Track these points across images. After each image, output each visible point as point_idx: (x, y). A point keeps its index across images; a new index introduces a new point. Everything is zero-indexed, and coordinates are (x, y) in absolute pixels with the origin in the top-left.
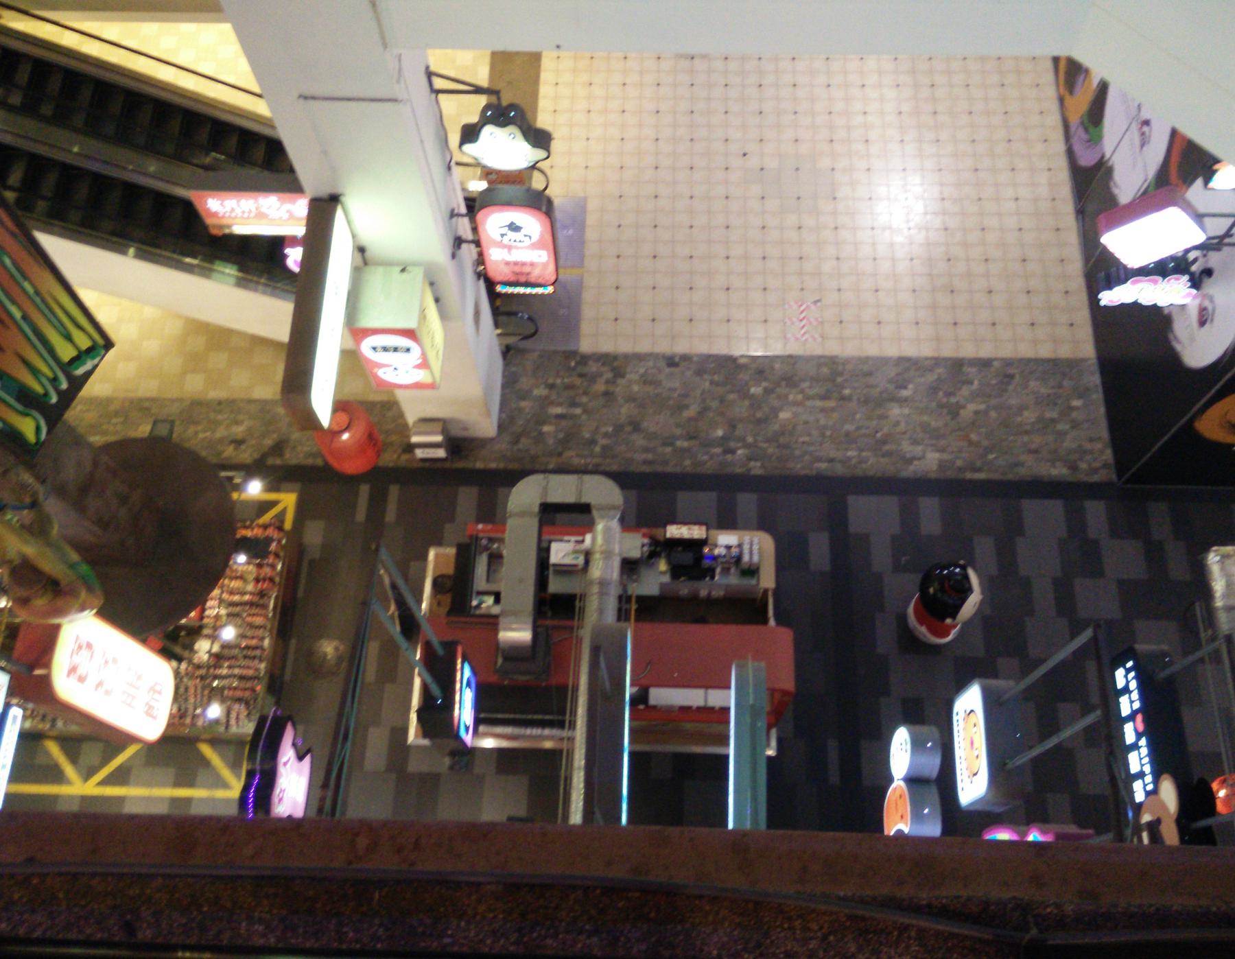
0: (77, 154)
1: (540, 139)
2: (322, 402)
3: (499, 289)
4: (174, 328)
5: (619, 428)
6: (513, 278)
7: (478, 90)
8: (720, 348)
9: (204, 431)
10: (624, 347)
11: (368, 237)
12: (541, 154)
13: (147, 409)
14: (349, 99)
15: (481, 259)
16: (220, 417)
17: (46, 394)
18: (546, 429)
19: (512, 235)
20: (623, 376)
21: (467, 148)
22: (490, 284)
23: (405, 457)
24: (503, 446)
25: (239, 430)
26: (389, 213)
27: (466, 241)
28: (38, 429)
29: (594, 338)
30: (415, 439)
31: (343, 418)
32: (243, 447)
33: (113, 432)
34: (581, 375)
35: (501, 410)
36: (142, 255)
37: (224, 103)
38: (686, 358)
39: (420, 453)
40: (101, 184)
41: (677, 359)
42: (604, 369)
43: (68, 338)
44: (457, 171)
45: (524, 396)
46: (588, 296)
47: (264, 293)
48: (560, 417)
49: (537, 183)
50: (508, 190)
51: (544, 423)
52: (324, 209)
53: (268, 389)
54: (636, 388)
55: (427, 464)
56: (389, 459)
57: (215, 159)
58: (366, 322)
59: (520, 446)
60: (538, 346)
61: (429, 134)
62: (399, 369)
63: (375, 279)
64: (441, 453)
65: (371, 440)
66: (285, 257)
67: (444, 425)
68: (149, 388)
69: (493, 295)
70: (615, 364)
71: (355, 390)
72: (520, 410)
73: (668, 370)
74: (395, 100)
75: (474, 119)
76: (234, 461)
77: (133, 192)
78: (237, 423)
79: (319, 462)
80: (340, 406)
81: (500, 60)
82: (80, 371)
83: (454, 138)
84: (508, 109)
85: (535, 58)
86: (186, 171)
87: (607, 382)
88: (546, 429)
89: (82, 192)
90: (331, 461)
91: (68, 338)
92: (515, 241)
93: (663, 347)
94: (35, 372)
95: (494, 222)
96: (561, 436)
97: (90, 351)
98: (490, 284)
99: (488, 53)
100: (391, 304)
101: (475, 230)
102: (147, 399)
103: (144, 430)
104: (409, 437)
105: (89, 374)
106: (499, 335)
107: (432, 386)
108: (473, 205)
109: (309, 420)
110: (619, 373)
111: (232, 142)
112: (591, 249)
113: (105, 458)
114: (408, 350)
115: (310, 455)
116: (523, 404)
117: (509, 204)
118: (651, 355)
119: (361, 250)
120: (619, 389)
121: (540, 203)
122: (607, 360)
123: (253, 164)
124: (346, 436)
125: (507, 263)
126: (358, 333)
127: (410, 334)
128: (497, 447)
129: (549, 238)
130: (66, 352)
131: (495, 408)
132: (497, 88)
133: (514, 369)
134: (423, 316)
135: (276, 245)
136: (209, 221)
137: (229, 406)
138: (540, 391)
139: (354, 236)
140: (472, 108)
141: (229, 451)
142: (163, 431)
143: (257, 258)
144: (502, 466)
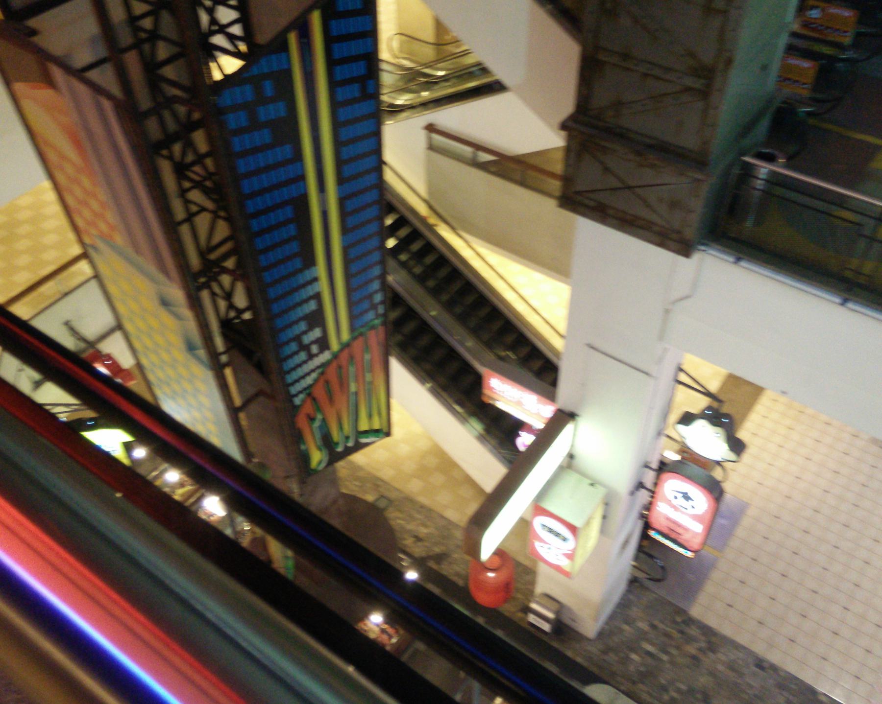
0: (433, 317)
1: (737, 446)
2: (491, 542)
3: (652, 533)
4: (423, 445)
5: (691, 691)
6: (666, 531)
7: (708, 394)
8: (807, 677)
9: (403, 519)
10: (726, 630)
11: (581, 453)
12: (732, 456)
13: (378, 486)
14: (620, 361)
15: (649, 507)
16: (418, 516)
17: (337, 444)
18: (634, 656)
19: (681, 501)
20: (714, 651)
21: (681, 428)
22: (647, 526)
23: (520, 615)
24: (594, 649)
25: (423, 531)
26: (603, 444)
27: (646, 488)
28: (320, 462)
29: (706, 608)
30: (534, 606)
31: (497, 561)
32: (420, 544)
33: (350, 487)
34: (681, 632)
35: (607, 623)
36: (434, 392)
37: (534, 329)
38: (774, 668)
39: (532, 618)
40: (438, 341)
41: (765, 665)
42: (703, 638)
43: (370, 416)
44: (664, 439)
45: (629, 621)
46: (716, 575)
47: (491, 451)
48: (649, 653)
49: (718, 474)
50: (694, 469)
51: (632, 649)
52: (563, 418)
53: (459, 513)
54: (720, 667)
55: (532, 629)
56: (508, 609)
57: (508, 355)
58: (548, 506)
59: (606, 657)
60: (660, 591)
61: (659, 405)
62: (551, 550)
63: (570, 479)
64: (546, 627)
65: (506, 589)
66: (519, 435)
67: (560, 608)
68: (387, 474)
69: (645, 536)
70: (713, 640)
71: (513, 549)
72: (621, 630)
73: (754, 669)
74: (647, 374)
75: (694, 410)
76: (408, 550)
77: (452, 354)
78: (426, 526)
79: (461, 583)
80: (500, 553)
81: (733, 381)
82: (364, 440)
83: (674, 416)
84: (722, 415)
85: (757, 391)
86: (490, 356)
87: (700, 649)
88: (634, 656)
89: (424, 341)
90: (472, 587)
91: (370, 416)
92: (683, 508)
93: (759, 648)
94: (341, 428)
95: (672, 485)
96: (642, 669)
97: (376, 432)
98: (647, 526)
99: (724, 372)
100: (569, 503)
101: (656, 484)
102: (382, 481)
103: (370, 498)
104: (530, 601)
105: (367, 445)
106: (634, 566)
107: (567, 574)
108: (663, 467)
109: (474, 548)
110: (712, 648)
111: (524, 351)
112: (735, 543)
113: (341, 502)
114: (565, 539)
115: (457, 574)
116: (626, 627)
117: (690, 478)
118: (744, 648)
119: (571, 456)
120: (708, 660)
121: (715, 489)
122: (707, 631)
123: (530, 370)
124: (491, 575)
125: (668, 519)
126: (538, 509)
127: (573, 529)
128: (589, 648)
129: (708, 517)
130: (364, 426)
131: (603, 618)
132: (721, 397)
133: (631, 597)
134: (588, 523)
135: (517, 426)
136: (486, 391)
137: (427, 512)
138: (643, 625)
139: (572, 446)
140: (699, 403)
141: (409, 542)
142: (382, 504)
143: (501, 429)
144: (585, 664)
